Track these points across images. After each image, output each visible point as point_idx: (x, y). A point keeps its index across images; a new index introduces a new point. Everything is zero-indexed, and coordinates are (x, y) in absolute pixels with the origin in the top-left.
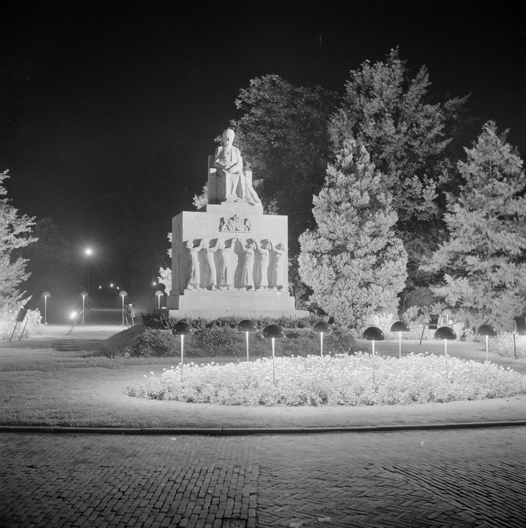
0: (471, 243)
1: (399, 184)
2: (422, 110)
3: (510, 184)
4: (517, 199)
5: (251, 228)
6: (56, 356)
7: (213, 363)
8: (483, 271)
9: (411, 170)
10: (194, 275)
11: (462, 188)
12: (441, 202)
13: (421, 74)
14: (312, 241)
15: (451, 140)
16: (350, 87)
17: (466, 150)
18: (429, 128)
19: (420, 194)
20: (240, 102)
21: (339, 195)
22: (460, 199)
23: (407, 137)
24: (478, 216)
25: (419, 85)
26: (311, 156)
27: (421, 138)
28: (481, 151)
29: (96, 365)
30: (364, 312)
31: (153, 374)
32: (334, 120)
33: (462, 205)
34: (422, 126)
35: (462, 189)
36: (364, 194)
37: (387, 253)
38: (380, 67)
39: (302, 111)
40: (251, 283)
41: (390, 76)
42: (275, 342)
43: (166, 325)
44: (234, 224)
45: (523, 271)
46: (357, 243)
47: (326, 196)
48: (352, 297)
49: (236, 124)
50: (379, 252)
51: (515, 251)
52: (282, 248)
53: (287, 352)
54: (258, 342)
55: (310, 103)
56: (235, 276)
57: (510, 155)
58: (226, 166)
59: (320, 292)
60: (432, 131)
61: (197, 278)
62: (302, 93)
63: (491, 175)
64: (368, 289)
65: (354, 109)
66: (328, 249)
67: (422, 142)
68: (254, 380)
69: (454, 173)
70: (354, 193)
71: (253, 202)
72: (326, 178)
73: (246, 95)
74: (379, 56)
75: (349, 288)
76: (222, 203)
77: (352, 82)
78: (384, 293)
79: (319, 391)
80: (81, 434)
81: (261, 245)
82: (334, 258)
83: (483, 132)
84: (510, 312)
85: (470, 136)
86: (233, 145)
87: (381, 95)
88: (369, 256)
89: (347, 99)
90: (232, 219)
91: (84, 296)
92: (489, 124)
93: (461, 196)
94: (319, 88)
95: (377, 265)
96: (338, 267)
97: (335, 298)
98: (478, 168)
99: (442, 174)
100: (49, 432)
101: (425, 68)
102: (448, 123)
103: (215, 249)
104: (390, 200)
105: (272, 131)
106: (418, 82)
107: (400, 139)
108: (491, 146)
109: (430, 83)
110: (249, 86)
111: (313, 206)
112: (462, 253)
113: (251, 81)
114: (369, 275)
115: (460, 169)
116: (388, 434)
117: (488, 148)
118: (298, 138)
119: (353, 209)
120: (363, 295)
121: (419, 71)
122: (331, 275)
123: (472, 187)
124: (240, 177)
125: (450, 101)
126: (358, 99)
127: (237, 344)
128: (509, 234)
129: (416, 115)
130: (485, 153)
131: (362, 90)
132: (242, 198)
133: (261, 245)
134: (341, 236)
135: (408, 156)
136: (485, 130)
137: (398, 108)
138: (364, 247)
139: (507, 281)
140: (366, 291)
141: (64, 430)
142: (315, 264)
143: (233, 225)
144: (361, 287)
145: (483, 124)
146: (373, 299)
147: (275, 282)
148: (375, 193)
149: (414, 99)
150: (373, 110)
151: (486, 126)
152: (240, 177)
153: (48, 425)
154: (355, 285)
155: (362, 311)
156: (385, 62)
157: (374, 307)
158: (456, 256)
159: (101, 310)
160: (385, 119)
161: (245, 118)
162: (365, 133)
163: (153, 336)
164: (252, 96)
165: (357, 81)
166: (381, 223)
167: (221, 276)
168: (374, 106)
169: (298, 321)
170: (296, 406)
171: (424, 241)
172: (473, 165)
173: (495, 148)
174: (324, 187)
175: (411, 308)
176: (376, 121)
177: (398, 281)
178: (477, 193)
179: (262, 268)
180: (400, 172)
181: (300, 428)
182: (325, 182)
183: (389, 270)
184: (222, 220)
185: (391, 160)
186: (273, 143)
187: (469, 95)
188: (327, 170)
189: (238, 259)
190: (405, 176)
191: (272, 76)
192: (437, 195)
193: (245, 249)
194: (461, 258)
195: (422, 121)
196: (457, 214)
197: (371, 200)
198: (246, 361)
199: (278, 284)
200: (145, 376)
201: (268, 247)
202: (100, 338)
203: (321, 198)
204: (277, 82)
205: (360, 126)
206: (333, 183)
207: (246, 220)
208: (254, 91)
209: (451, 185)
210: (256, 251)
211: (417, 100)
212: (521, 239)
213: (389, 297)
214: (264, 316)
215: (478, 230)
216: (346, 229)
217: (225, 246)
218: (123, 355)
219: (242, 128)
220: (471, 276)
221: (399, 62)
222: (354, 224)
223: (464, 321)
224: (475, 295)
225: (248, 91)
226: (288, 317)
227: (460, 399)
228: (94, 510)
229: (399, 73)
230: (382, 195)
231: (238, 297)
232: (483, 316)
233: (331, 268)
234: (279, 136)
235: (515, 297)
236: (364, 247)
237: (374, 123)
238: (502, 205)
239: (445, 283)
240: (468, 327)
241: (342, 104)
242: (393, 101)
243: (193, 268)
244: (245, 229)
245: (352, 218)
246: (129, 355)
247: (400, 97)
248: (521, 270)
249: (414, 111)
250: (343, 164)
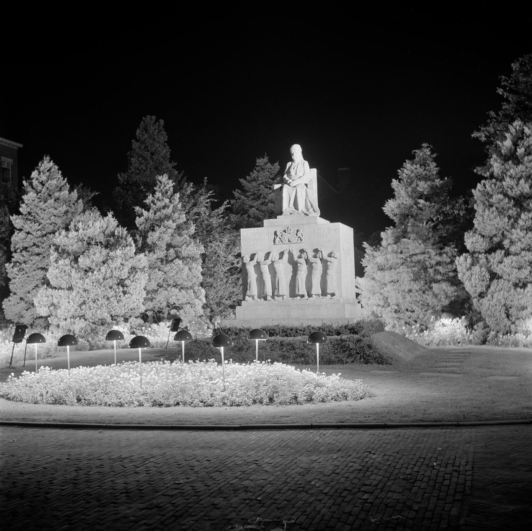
5: (302, 238)
44: (286, 236)
61: (254, 289)
90: (285, 231)
103: (269, 262)
184: (275, 233)
189: (292, 269)
199: (300, 293)
201: (318, 255)
228: (427, 508)
243: (249, 280)
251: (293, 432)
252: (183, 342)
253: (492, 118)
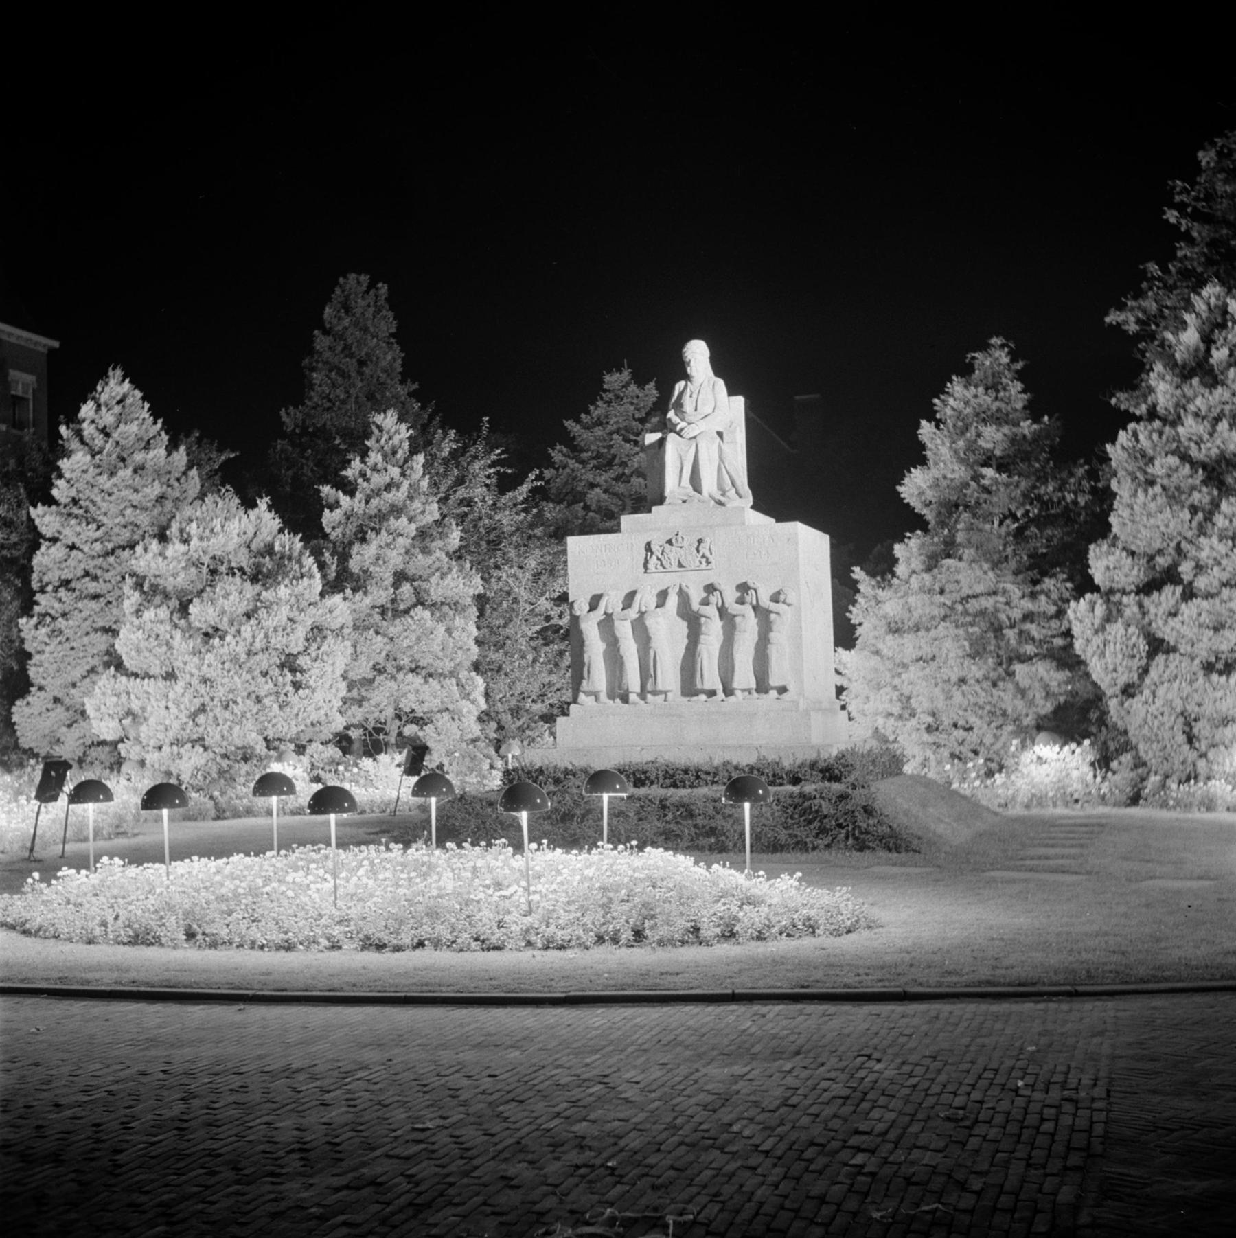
5: (711, 558)
42: (529, 820)
44: (673, 554)
61: (598, 677)
90: (670, 542)
103: (633, 613)
143: (671, 556)
184: (648, 548)
189: (686, 631)
199: (707, 686)
201: (748, 598)
207: (700, 541)
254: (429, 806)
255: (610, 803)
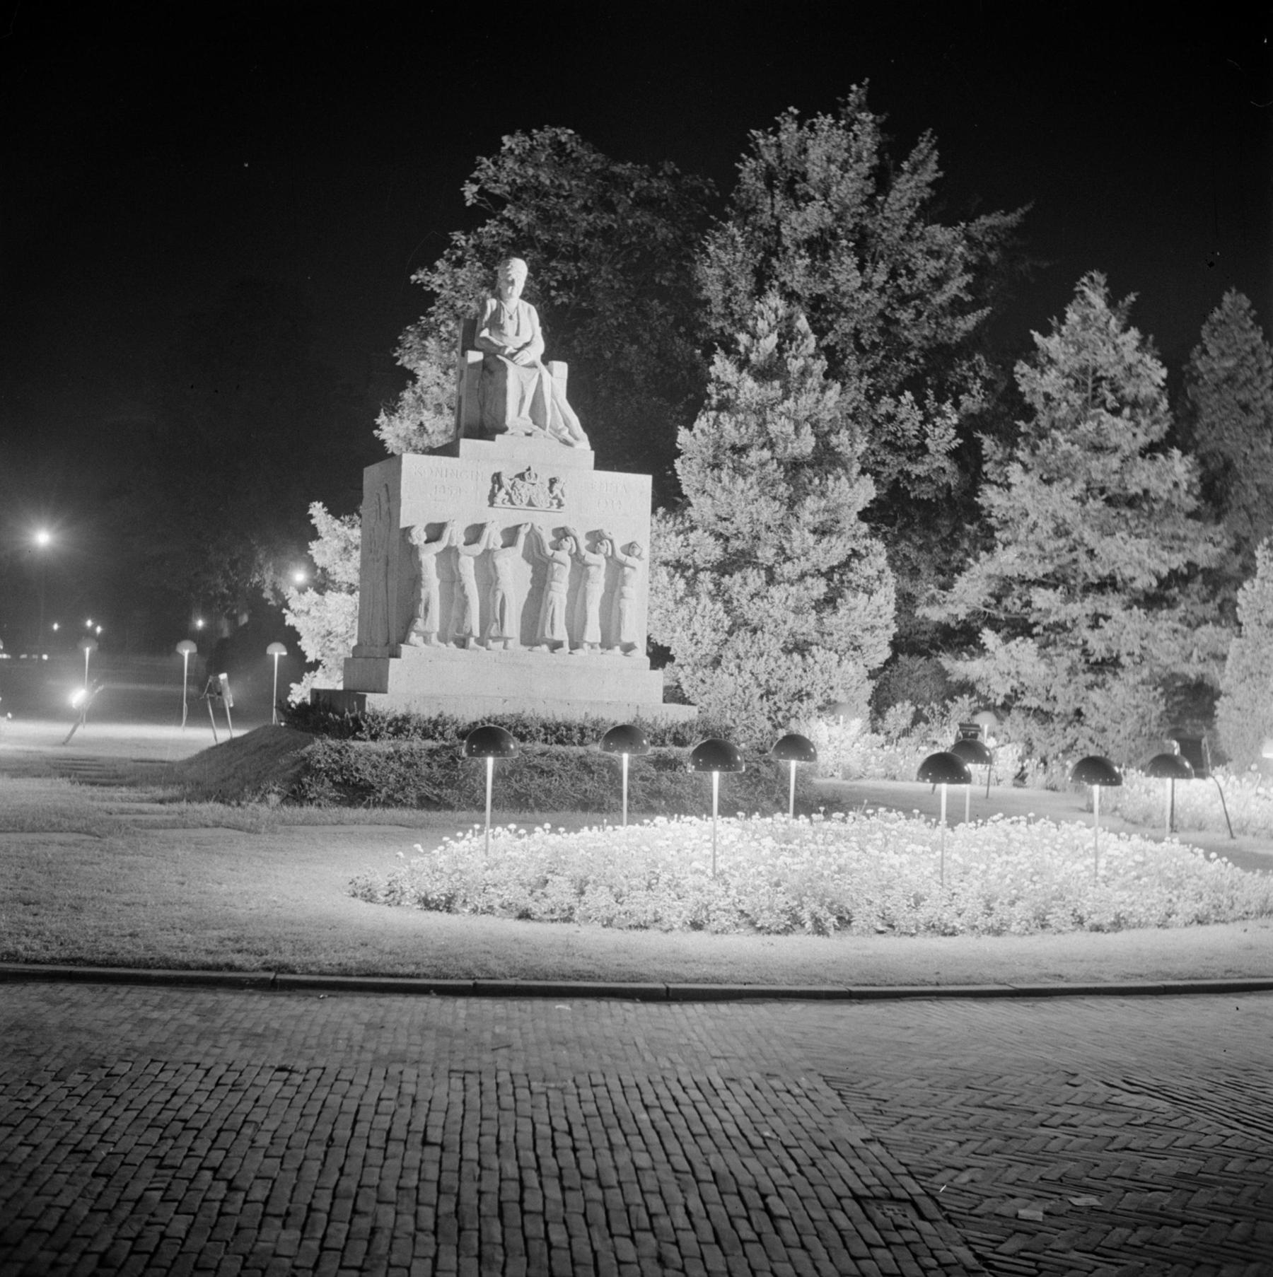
0: (1045, 558)
1: (864, 409)
2: (921, 238)
3: (1138, 424)
4: (1154, 458)
5: (564, 501)
6: (92, 798)
7: (547, 826)
8: (1069, 625)
9: (893, 377)
10: (426, 610)
11: (1022, 426)
12: (967, 457)
13: (920, 151)
14: (674, 538)
15: (987, 311)
16: (748, 170)
17: (1037, 337)
18: (938, 283)
19: (915, 436)
20: (475, 188)
21: (743, 430)
22: (1019, 454)
23: (885, 298)
24: (1064, 495)
25: (916, 177)
26: (652, 330)
27: (918, 302)
28: (1073, 343)
29: (210, 823)
30: (793, 712)
31: (421, 850)
32: (711, 248)
33: (1026, 469)
34: (921, 275)
35: (1022, 429)
36: (803, 431)
37: (851, 575)
38: (826, 128)
39: (630, 222)
40: (561, 634)
41: (848, 150)
43: (360, 728)
44: (524, 489)
45: (1160, 629)
46: (782, 549)
47: (712, 431)
48: (766, 676)
49: (464, 243)
50: (832, 569)
51: (1145, 581)
52: (637, 552)
53: (654, 803)
54: (586, 778)
55: (645, 202)
56: (523, 616)
57: (1138, 355)
58: (505, 347)
59: (690, 660)
60: (946, 287)
61: (432, 619)
62: (629, 178)
63: (1095, 400)
64: (803, 656)
65: (759, 223)
66: (712, 558)
67: (919, 313)
68: (664, 869)
69: (994, 391)
70: (780, 427)
71: (570, 439)
72: (711, 388)
73: (491, 173)
74: (820, 100)
75: (762, 655)
76: (498, 437)
77: (756, 159)
78: (843, 669)
79: (828, 900)
80: (334, 993)
81: (588, 542)
82: (726, 580)
83: (1075, 297)
84: (1129, 721)
85: (1048, 305)
86: (523, 297)
87: (826, 196)
88: (809, 580)
89: (742, 200)
91: (87, 650)
92: (1091, 279)
93: (1022, 444)
94: (669, 167)
95: (829, 601)
96: (735, 603)
97: (726, 676)
98: (1064, 382)
99: (969, 391)
100: (250, 987)
101: (932, 136)
102: (979, 270)
103: (478, 549)
104: (861, 447)
105: (553, 264)
106: (914, 170)
107: (868, 302)
108: (1094, 334)
109: (941, 174)
110: (498, 152)
111: (678, 454)
112: (1023, 581)
113: (505, 139)
114: (807, 625)
115: (1022, 381)
116: (1046, 1004)
117: (1087, 337)
118: (617, 286)
119: (775, 465)
120: (792, 673)
121: (917, 144)
122: (719, 621)
123: (1048, 426)
124: (540, 376)
125: (983, 219)
126: (769, 201)
127: (539, 781)
128: (1133, 540)
129: (908, 248)
130: (1080, 347)
131: (777, 179)
132: (544, 429)
133: (588, 542)
134: (746, 530)
135: (885, 344)
136: (1082, 292)
137: (864, 227)
138: (798, 558)
139: (1123, 652)
140: (801, 664)
141: (280, 982)
142: (681, 593)
143: (522, 491)
144: (787, 651)
145: (1078, 280)
146: (816, 681)
147: (619, 634)
148: (826, 429)
149: (903, 209)
150: (804, 229)
151: (1084, 284)
152: (540, 376)
153: (240, 969)
154: (775, 647)
155: (788, 710)
156: (837, 117)
157: (819, 700)
158: (1005, 586)
159: (144, 687)
160: (838, 256)
161: (487, 228)
162: (784, 284)
163: (336, 756)
164: (503, 176)
165: (767, 157)
166: (840, 501)
167: (492, 616)
168: (806, 220)
169: (674, 730)
170: (778, 933)
171: (920, 548)
172: (1053, 373)
173: (1104, 337)
174: (706, 409)
175: (898, 706)
176: (812, 256)
177: (875, 641)
178: (1061, 439)
179: (589, 598)
180: (866, 381)
181: (841, 988)
182: (709, 396)
183: (855, 614)
184: (497, 478)
185: (848, 351)
186: (553, 293)
187: (1027, 208)
188: (712, 369)
189: (530, 575)
190: (880, 393)
191: (558, 131)
192: (960, 441)
193: (549, 552)
194: (1015, 593)
195: (921, 262)
196: (1013, 489)
197: (817, 446)
198: (621, 823)
199: (626, 638)
200: (401, 854)
201: (603, 549)
202: (168, 756)
203: (699, 435)
204: (569, 146)
205: (770, 266)
206: (728, 399)
207: (553, 482)
208: (510, 164)
209: (988, 418)
210: (576, 557)
211: (910, 213)
212: (1160, 552)
213: (851, 677)
214: (594, 715)
215: (1061, 531)
216: (758, 513)
217: (501, 542)
218: (263, 800)
219: (477, 251)
220: (1038, 635)
221: (871, 117)
222: (778, 503)
223: (1022, 740)
224: (1050, 680)
225: (495, 163)
226: (650, 721)
227: (1140, 925)
229: (869, 146)
230: (844, 436)
231: (530, 666)
232: (1065, 729)
233: (719, 605)
234: (569, 277)
235: (1141, 688)
236: (798, 558)
237: (808, 261)
238: (1116, 472)
239: (982, 649)
240: (1029, 754)
241: (728, 209)
242: (853, 210)
243: (423, 592)
244: (551, 504)
245: (773, 485)
246: (278, 801)
247: (870, 201)
248: (1157, 626)
249: (902, 238)
250: (753, 357)
251: (797, 1008)
252: (626, 757)
253: (456, 247)
254: (939, 795)
255: (948, 795)
